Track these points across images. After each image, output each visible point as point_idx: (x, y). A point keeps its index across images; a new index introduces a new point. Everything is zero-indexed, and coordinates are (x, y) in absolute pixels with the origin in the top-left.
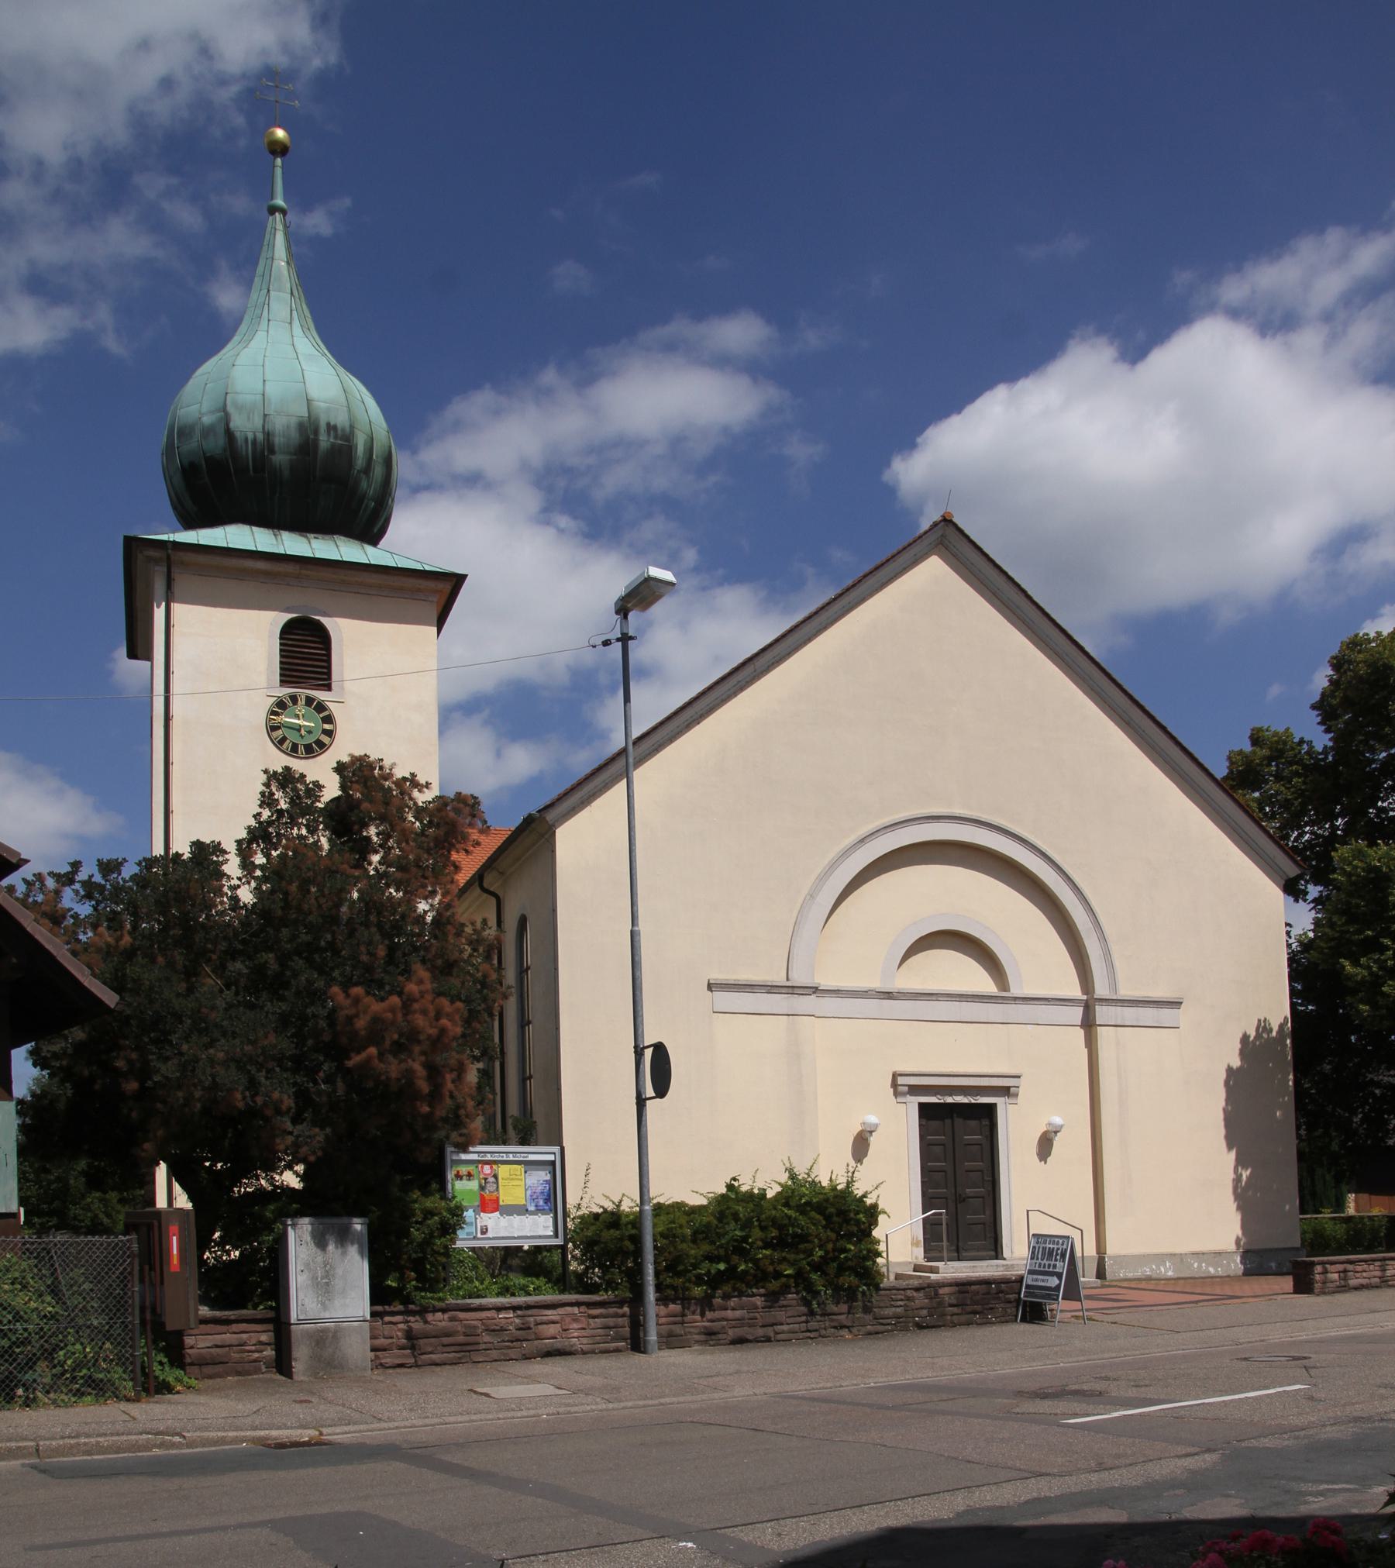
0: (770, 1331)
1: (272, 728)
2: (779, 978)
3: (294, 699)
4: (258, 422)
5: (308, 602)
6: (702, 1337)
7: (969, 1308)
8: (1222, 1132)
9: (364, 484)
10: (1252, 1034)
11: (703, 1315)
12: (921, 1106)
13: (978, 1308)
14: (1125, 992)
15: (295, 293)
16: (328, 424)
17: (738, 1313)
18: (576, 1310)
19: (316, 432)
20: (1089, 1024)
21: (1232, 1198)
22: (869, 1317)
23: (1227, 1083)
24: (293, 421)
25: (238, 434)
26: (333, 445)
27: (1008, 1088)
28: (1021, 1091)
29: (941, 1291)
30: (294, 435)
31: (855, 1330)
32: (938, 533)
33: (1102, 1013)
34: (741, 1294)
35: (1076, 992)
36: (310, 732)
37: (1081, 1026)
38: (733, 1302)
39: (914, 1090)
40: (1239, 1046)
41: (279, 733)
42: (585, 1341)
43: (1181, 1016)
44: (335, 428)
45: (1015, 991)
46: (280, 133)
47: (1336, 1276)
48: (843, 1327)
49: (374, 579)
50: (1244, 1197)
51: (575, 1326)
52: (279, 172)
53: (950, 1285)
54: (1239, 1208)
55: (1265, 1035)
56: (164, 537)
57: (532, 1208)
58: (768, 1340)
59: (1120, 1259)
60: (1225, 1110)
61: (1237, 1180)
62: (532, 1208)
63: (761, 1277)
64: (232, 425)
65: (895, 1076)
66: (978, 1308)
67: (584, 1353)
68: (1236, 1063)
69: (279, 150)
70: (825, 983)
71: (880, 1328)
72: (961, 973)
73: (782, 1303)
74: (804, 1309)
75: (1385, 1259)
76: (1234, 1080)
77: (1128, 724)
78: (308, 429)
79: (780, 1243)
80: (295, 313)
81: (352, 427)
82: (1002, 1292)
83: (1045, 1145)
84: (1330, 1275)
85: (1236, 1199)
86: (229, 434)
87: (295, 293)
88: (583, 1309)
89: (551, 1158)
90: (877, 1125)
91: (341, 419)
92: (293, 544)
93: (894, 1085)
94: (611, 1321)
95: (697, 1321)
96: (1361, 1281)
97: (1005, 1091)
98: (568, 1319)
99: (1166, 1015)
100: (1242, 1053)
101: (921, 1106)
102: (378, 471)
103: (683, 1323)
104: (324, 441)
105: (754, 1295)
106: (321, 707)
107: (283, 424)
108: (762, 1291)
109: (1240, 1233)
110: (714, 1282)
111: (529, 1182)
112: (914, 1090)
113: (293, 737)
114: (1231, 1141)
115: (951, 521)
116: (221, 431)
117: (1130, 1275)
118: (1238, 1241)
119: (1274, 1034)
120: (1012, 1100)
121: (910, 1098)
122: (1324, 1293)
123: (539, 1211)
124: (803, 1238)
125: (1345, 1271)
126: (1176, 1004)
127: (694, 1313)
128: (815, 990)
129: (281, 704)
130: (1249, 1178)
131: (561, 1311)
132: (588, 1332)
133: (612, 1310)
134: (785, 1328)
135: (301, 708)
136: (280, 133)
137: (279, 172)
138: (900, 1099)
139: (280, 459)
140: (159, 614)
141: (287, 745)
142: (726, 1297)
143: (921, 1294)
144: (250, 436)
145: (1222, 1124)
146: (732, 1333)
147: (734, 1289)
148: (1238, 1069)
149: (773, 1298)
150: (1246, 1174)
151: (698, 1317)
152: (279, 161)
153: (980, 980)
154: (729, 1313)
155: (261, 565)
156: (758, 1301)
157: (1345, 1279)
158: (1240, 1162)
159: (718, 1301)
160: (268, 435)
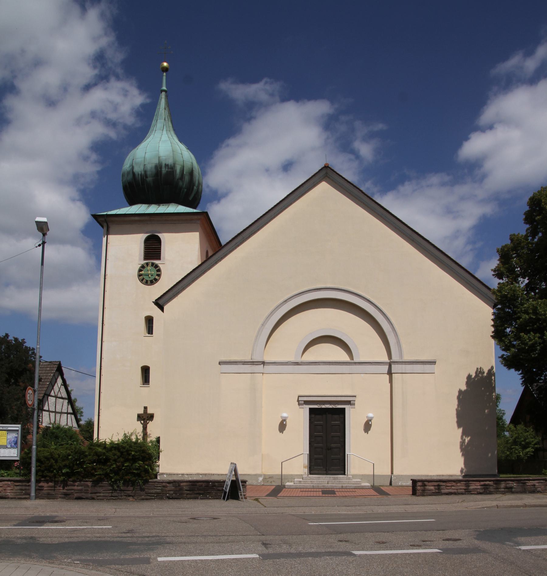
0: (93, 495)
1: (140, 275)
2: (248, 359)
3: (147, 264)
4: (142, 167)
5: (152, 229)
6: (63, 496)
7: (196, 492)
8: (456, 420)
9: (181, 183)
10: (473, 375)
11: (64, 488)
12: (311, 409)
13: (202, 492)
14: (406, 358)
15: (167, 119)
16: (165, 164)
17: (80, 488)
18: (9, 483)
19: (161, 168)
20: (390, 373)
21: (459, 450)
22: (142, 493)
23: (458, 398)
24: (153, 165)
25: (136, 173)
26: (167, 171)
27: (350, 401)
28: (356, 403)
29: (182, 484)
30: (154, 170)
31: (136, 497)
32: (323, 172)
33: (395, 368)
34: (80, 481)
35: (386, 359)
36: (152, 275)
37: (388, 374)
38: (77, 484)
39: (306, 403)
40: (466, 380)
41: (141, 277)
42: (12, 494)
43: (435, 368)
44: (168, 165)
45: (356, 360)
46: (165, 64)
47: (432, 488)
48: (129, 496)
49: (175, 218)
50: (465, 450)
51: (9, 488)
52: (164, 78)
53: (187, 482)
54: (463, 455)
55: (480, 375)
56: (105, 213)
57: (9, 446)
58: (93, 499)
59: (285, 475)
60: (457, 410)
61: (462, 443)
62: (9, 446)
63: (88, 474)
64: (134, 170)
65: (299, 397)
66: (202, 492)
67: (12, 498)
68: (464, 388)
69: (165, 70)
70: (267, 359)
71: (148, 497)
72: (335, 353)
73: (100, 485)
74: (110, 488)
75: (469, 481)
76: (462, 396)
77: (413, 241)
78: (158, 167)
79: (99, 462)
80: (165, 127)
81: (174, 164)
82: (215, 486)
83: (367, 427)
84: (427, 487)
85: (461, 451)
86: (134, 174)
87: (167, 119)
88: (12, 482)
89: (17, 429)
90: (372, 418)
91: (170, 162)
92: (153, 209)
93: (298, 401)
94: (24, 488)
95: (60, 489)
96: (450, 491)
97: (349, 403)
98: (6, 486)
99: (428, 368)
100: (467, 383)
101: (310, 409)
102: (187, 178)
103: (54, 490)
104: (164, 170)
105: (86, 481)
106: (156, 266)
107: (150, 166)
108: (91, 480)
109: (463, 466)
110: (67, 475)
111: (8, 437)
112: (306, 403)
113: (146, 278)
114: (459, 424)
115: (328, 167)
116: (131, 173)
117: (404, 484)
118: (462, 471)
119: (485, 374)
120: (353, 407)
121: (305, 406)
122: (423, 495)
123: (12, 447)
124: (107, 460)
125: (438, 485)
126: (434, 363)
127: (60, 486)
128: (263, 363)
129: (143, 267)
130: (469, 442)
131: (3, 483)
132: (14, 491)
133: (24, 484)
134: (102, 494)
135: (149, 268)
136: (165, 64)
137: (164, 78)
138: (301, 407)
139: (149, 179)
140: (104, 239)
141: (144, 281)
142: (74, 481)
143: (171, 485)
144: (140, 173)
145: (455, 416)
146: (76, 495)
147: (78, 479)
148: (465, 391)
149: (96, 483)
150: (467, 440)
151: (62, 488)
152: (165, 74)
153: (343, 356)
154: (76, 488)
155: (137, 218)
156: (90, 484)
157: (439, 489)
158: (464, 433)
159: (69, 483)
160: (145, 172)
